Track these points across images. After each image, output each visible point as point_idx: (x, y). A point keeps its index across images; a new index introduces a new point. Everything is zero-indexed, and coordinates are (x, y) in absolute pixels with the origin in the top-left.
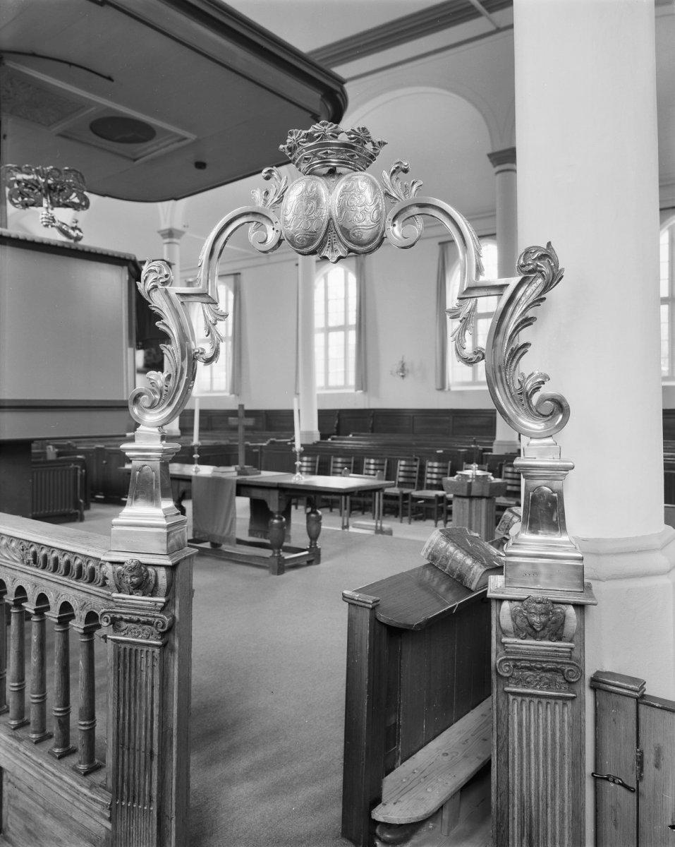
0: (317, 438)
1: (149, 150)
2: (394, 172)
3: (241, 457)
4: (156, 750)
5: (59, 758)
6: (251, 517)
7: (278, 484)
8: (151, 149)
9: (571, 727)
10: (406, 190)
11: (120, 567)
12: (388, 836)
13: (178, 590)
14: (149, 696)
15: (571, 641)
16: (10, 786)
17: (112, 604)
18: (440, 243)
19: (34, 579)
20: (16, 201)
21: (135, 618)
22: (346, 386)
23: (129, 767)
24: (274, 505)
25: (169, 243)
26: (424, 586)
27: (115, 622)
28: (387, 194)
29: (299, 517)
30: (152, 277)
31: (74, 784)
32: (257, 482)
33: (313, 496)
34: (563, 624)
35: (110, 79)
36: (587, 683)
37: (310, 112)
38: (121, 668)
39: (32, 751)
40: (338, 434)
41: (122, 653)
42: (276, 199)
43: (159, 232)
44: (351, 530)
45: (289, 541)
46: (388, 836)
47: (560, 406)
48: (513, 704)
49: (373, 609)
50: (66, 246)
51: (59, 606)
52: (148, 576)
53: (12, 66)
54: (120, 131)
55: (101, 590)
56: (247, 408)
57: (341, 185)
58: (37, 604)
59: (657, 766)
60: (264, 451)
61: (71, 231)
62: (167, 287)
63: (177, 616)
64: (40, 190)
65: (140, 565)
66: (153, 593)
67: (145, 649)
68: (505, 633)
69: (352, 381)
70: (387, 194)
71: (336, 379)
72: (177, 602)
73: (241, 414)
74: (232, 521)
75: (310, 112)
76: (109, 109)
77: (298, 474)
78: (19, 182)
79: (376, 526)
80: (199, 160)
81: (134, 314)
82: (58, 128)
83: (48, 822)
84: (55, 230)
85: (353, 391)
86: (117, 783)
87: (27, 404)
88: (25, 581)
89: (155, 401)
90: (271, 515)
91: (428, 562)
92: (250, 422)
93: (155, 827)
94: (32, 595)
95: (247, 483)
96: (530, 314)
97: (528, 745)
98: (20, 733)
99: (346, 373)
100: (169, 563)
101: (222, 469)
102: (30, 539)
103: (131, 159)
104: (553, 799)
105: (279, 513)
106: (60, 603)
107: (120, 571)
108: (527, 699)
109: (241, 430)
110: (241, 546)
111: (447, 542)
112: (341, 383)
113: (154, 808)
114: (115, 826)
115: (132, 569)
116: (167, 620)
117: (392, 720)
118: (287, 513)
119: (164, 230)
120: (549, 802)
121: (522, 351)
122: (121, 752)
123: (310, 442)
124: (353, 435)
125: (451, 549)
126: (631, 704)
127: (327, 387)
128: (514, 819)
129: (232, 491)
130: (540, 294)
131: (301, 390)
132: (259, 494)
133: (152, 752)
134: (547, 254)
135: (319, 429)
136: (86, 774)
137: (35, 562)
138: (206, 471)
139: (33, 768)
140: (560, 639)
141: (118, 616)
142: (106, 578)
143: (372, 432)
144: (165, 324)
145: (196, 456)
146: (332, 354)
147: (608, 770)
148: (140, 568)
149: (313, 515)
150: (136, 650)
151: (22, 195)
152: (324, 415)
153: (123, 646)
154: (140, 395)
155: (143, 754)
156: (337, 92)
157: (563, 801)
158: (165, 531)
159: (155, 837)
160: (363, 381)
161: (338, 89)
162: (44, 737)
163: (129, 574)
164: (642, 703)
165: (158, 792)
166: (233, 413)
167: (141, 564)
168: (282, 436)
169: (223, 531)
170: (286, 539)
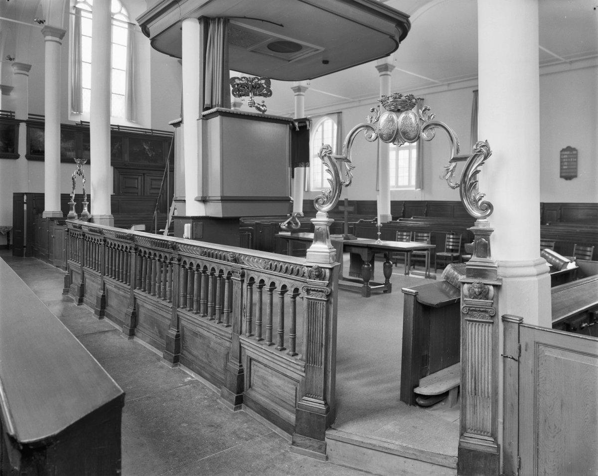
0: (390, 219)
1: (297, 56)
2: (424, 110)
3: (346, 229)
4: (324, 343)
6: (351, 265)
7: (368, 245)
8: (298, 56)
9: (492, 334)
11: (310, 269)
12: (422, 402)
14: (321, 321)
15: (492, 300)
16: (255, 367)
18: (474, 91)
19: (269, 276)
20: (235, 93)
21: (316, 289)
22: (409, 186)
24: (365, 256)
25: (298, 95)
26: (443, 291)
28: (421, 119)
29: (379, 266)
32: (355, 243)
33: (387, 252)
34: (488, 293)
35: (282, 25)
36: (500, 318)
37: (389, 35)
38: (310, 310)
40: (404, 217)
41: (310, 303)
43: (292, 88)
44: (411, 275)
45: (373, 279)
46: (422, 402)
47: (490, 206)
49: (415, 296)
50: (260, 116)
53: (233, 23)
55: (302, 278)
57: (403, 115)
58: (270, 287)
59: (526, 350)
60: (356, 226)
61: (261, 107)
63: (333, 289)
64: (248, 88)
65: (319, 267)
68: (466, 296)
69: (413, 182)
70: (421, 119)
71: (404, 181)
73: (346, 204)
75: (389, 35)
76: (279, 38)
77: (379, 239)
78: (238, 84)
79: (426, 274)
80: (325, 59)
81: (291, 147)
82: (250, 48)
84: (254, 108)
85: (414, 189)
88: (263, 277)
89: (325, 201)
90: (363, 262)
91: (445, 280)
92: (351, 209)
95: (349, 244)
96: (478, 169)
97: (475, 341)
98: (261, 342)
99: (409, 176)
100: (331, 267)
103: (287, 60)
105: (368, 261)
106: (281, 285)
107: (310, 271)
108: (474, 323)
109: (346, 213)
110: (345, 281)
111: (454, 270)
112: (406, 183)
113: (323, 367)
114: (306, 374)
115: (316, 269)
116: (329, 290)
117: (425, 353)
118: (372, 262)
119: (295, 87)
120: (483, 364)
122: (309, 344)
123: (386, 222)
124: (414, 218)
125: (456, 273)
126: (516, 326)
127: (398, 186)
129: (341, 249)
130: (483, 161)
131: (380, 188)
132: (355, 250)
133: (322, 344)
134: (486, 145)
135: (391, 213)
140: (487, 299)
143: (426, 216)
146: (401, 163)
147: (508, 354)
149: (387, 264)
151: (239, 90)
152: (394, 204)
153: (311, 301)
154: (319, 199)
156: (403, 23)
157: (489, 364)
158: (329, 254)
160: (421, 182)
161: (404, 21)
168: (368, 217)
170: (371, 278)
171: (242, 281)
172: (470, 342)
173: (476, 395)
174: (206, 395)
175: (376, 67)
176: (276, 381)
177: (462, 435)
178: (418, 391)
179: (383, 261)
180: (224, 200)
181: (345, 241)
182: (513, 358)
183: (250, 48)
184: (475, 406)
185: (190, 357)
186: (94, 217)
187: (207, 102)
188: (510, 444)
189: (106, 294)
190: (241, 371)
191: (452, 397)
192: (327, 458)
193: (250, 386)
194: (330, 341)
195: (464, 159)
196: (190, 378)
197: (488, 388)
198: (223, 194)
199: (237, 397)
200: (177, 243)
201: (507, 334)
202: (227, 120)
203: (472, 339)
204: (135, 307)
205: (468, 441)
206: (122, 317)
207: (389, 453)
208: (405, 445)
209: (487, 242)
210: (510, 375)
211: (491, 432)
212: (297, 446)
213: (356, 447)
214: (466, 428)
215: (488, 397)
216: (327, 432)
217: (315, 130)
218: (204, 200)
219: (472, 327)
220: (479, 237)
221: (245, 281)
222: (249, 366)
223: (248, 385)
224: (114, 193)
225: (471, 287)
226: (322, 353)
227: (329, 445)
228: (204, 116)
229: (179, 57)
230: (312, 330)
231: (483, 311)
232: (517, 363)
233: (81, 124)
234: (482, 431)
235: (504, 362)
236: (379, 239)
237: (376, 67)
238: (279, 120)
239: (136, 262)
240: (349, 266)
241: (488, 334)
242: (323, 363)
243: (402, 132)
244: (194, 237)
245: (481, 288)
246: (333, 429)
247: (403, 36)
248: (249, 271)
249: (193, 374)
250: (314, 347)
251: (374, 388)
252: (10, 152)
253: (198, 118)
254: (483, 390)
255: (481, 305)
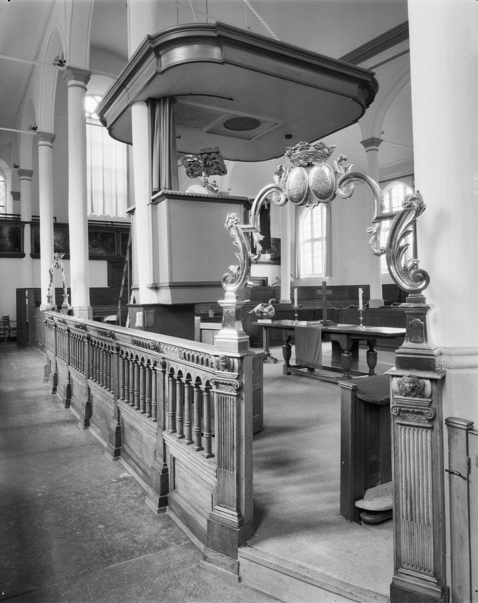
4: (235, 445)
5: (197, 451)
6: (332, 354)
10: (346, 169)
13: (244, 371)
14: (232, 419)
17: (215, 376)
19: (185, 366)
21: (225, 382)
23: (224, 453)
27: (217, 384)
29: (363, 353)
30: (231, 221)
31: (202, 461)
37: (352, 98)
39: (185, 447)
41: (220, 399)
42: (284, 180)
48: (401, 430)
51: (195, 378)
52: (230, 362)
54: (241, 126)
56: (328, 285)
57: (314, 170)
62: (237, 225)
66: (233, 370)
67: (230, 397)
68: (396, 393)
72: (244, 376)
74: (319, 354)
82: (207, 129)
83: (194, 483)
86: (219, 460)
87: (197, 284)
92: (330, 292)
93: (235, 481)
94: (185, 375)
97: (409, 452)
98: (181, 440)
101: (312, 322)
102: (183, 347)
104: (423, 480)
105: (347, 350)
108: (408, 428)
109: (324, 298)
113: (235, 473)
114: (218, 480)
115: (223, 359)
121: (405, 248)
128: (402, 489)
129: (319, 336)
132: (334, 337)
136: (207, 457)
137: (185, 358)
138: (303, 324)
139: (186, 456)
141: (217, 381)
142: (212, 363)
144: (236, 243)
145: (296, 315)
147: (454, 469)
148: (226, 358)
150: (226, 398)
153: (220, 395)
155: (230, 447)
159: (235, 487)
161: (370, 80)
162: (191, 442)
163: (221, 361)
164: (470, 433)
165: (237, 465)
166: (320, 288)
167: (227, 356)
169: (314, 360)
171: (164, 372)
172: (403, 451)
173: (412, 520)
174: (135, 494)
175: (362, 142)
176: (195, 484)
177: (396, 569)
178: (360, 504)
179: (366, 349)
180: (173, 286)
181: (324, 328)
182: (460, 475)
183: (207, 129)
184: (412, 534)
185: (128, 451)
186: (73, 309)
187: (155, 186)
188: (460, 588)
189: (71, 383)
190: (165, 471)
191: (383, 517)
192: (240, 579)
193: (174, 488)
194: (242, 443)
195: (390, 216)
196: (126, 474)
197: (428, 513)
198: (172, 279)
199: (160, 499)
200: (114, 331)
201: (453, 442)
202: (175, 203)
203: (405, 448)
204: (89, 397)
205: (404, 580)
206: (80, 406)
207: (313, 585)
208: (328, 574)
209: (423, 323)
210: (458, 497)
211: (433, 570)
212: (209, 562)
213: (271, 570)
214: (401, 561)
215: (429, 524)
216: (239, 549)
217: (304, 214)
218: (156, 288)
219: (405, 433)
220: (411, 317)
221: (167, 372)
222: (172, 465)
223: (172, 486)
224: (108, 286)
225: (401, 382)
226: (233, 458)
227: (242, 565)
228: (153, 200)
229: (130, 143)
230: (222, 429)
231: (417, 413)
232: (465, 482)
233: (112, 225)
234: (420, 567)
235: (450, 478)
236: (361, 325)
237: (362, 142)
238: (235, 200)
239: (89, 352)
240: (331, 355)
241: (426, 443)
242: (235, 468)
243: (314, 191)
244: (146, 328)
245: (413, 382)
246: (249, 546)
247: (370, 100)
248: (169, 361)
249: (130, 470)
250: (225, 448)
251: (313, 497)
252: (16, 251)
253: (148, 203)
254: (421, 516)
255: (415, 405)
